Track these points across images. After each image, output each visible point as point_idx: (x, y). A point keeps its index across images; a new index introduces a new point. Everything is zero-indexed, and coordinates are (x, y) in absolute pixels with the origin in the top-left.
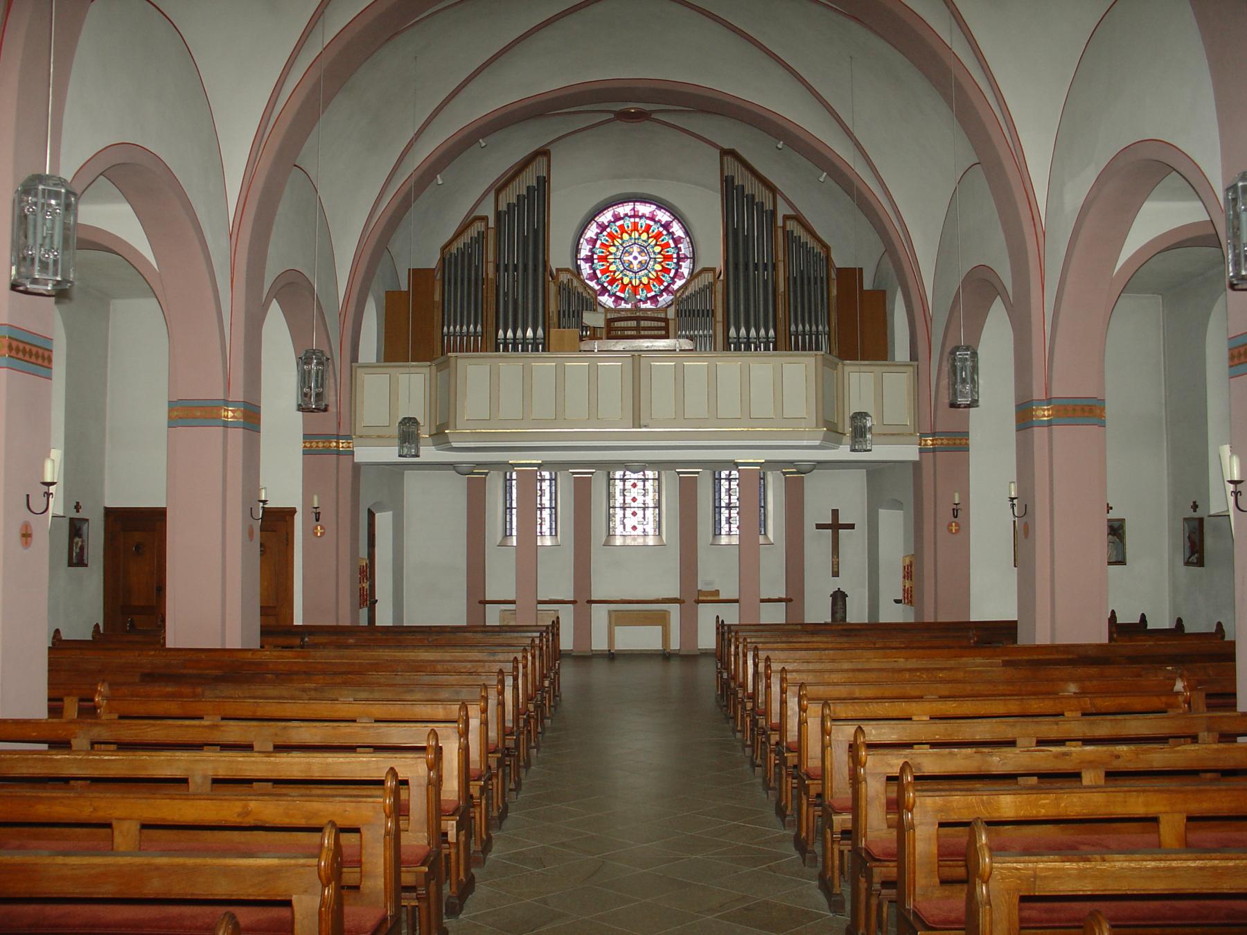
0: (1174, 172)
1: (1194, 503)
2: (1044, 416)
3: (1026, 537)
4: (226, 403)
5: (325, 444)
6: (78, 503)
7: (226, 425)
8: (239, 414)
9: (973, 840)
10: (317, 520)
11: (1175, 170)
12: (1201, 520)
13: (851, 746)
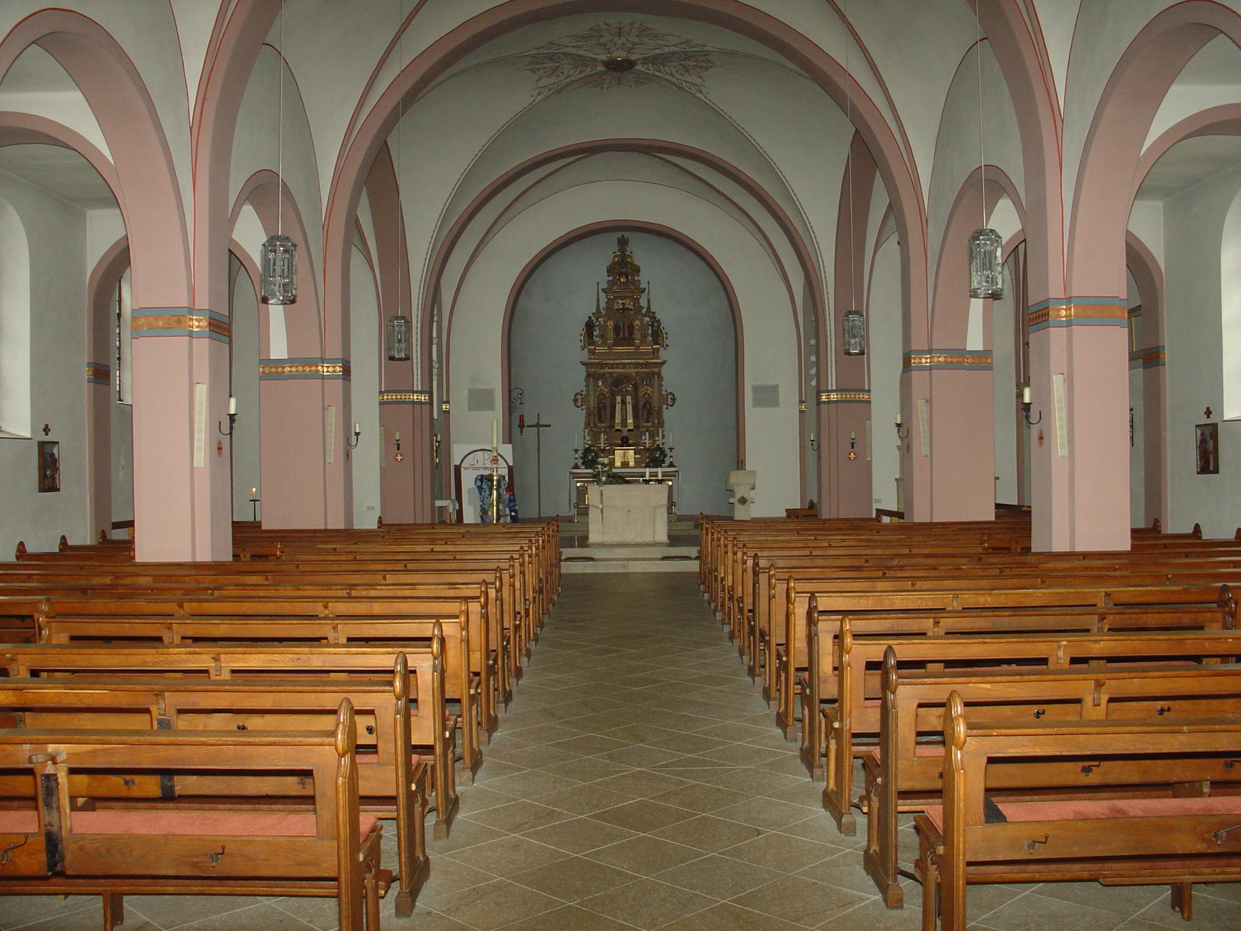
0: (1222, 35)
1: (1208, 408)
2: (927, 362)
3: (1041, 444)
4: (191, 310)
5: (201, 324)
6: (47, 426)
7: (191, 335)
8: (204, 323)
9: (949, 719)
10: (398, 449)
11: (1222, 32)
12: (1215, 426)
13: (836, 637)
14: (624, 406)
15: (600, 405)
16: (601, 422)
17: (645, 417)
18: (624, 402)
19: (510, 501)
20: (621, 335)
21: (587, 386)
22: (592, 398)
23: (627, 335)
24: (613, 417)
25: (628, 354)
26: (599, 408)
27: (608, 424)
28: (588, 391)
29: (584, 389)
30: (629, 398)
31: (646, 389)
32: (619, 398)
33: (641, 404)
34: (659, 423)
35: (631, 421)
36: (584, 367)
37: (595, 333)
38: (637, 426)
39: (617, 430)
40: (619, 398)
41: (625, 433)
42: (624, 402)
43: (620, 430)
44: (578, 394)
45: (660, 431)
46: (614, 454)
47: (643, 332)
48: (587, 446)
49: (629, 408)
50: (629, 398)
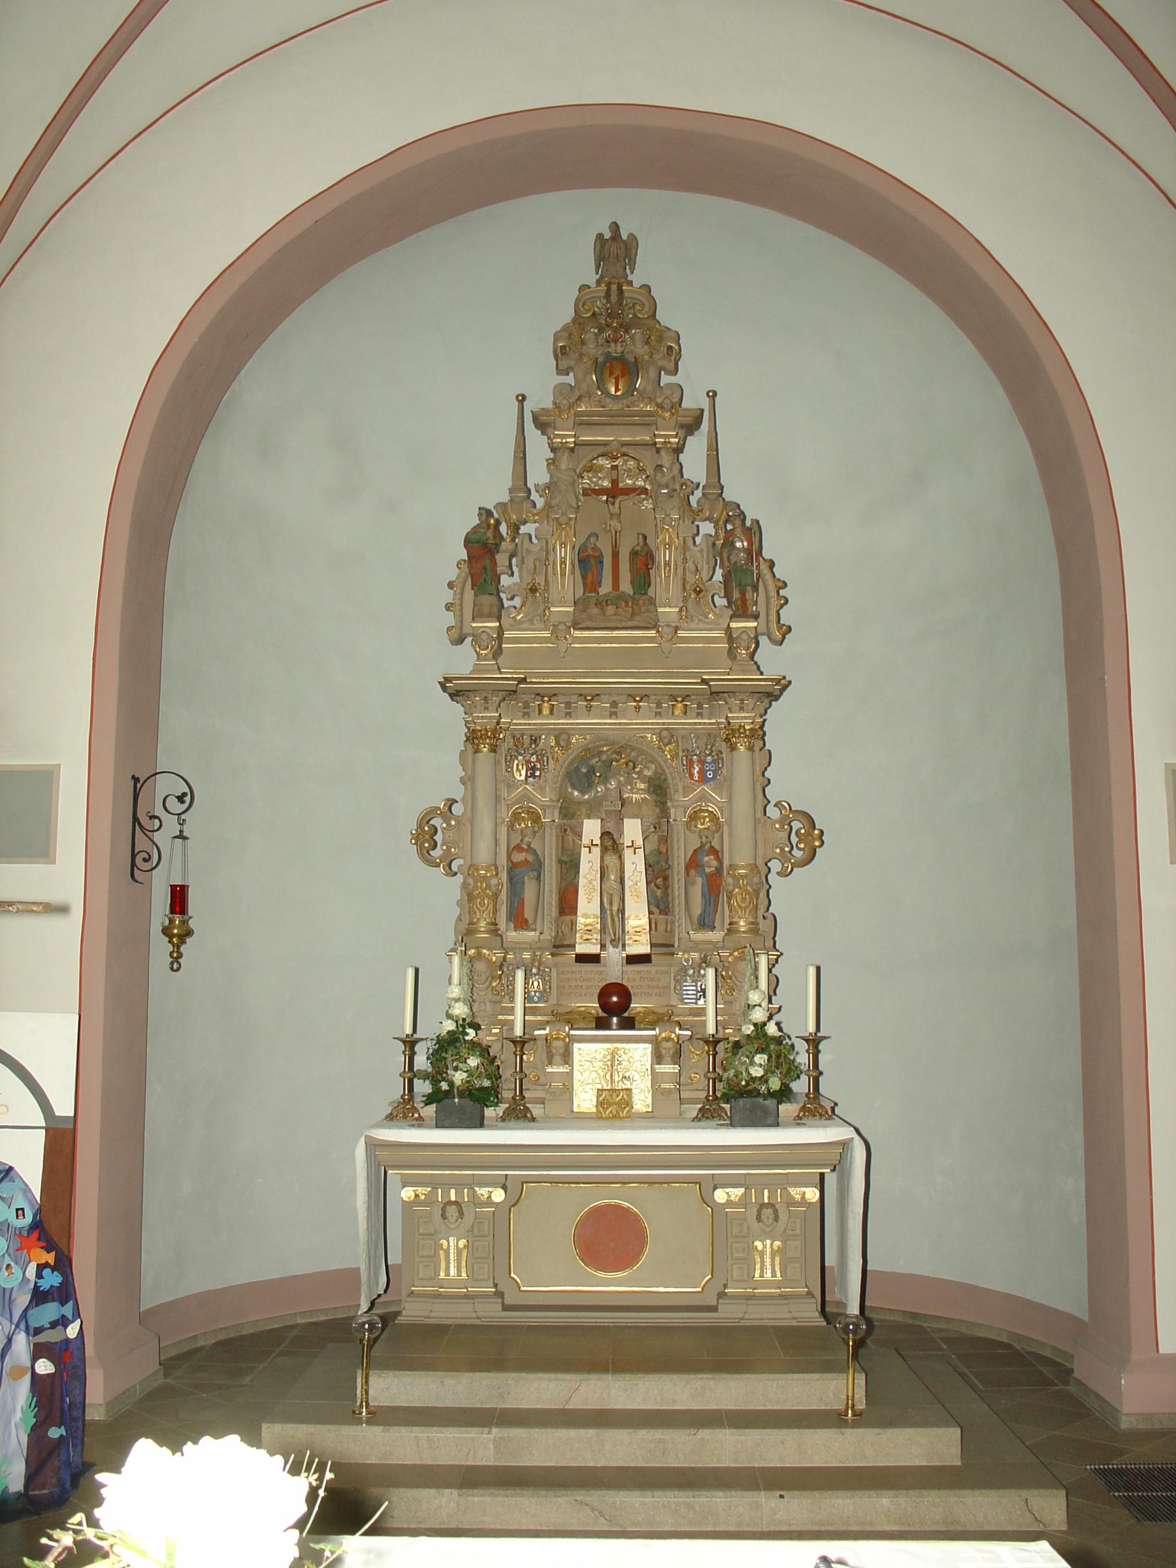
14: (611, 859)
15: (519, 857)
16: (520, 922)
17: (697, 910)
18: (611, 843)
19: (39, 1297)
20: (606, 588)
21: (468, 780)
22: (485, 824)
23: (626, 587)
24: (567, 904)
25: (631, 657)
26: (513, 867)
27: (548, 935)
28: (471, 800)
29: (458, 792)
30: (632, 830)
31: (703, 797)
32: (591, 829)
33: (681, 851)
34: (754, 929)
35: (644, 921)
36: (457, 709)
37: (505, 580)
38: (663, 945)
39: (582, 958)
40: (591, 829)
41: (614, 967)
42: (611, 843)
43: (594, 959)
44: (432, 812)
45: (763, 961)
46: (567, 1058)
47: (691, 579)
48: (450, 1026)
49: (635, 866)
50: (632, 830)
